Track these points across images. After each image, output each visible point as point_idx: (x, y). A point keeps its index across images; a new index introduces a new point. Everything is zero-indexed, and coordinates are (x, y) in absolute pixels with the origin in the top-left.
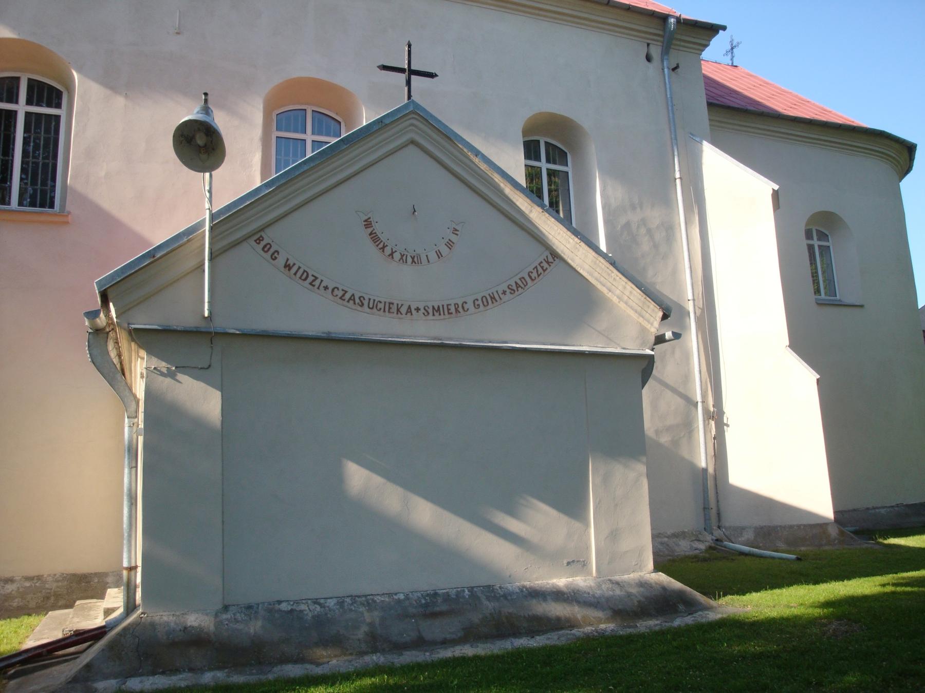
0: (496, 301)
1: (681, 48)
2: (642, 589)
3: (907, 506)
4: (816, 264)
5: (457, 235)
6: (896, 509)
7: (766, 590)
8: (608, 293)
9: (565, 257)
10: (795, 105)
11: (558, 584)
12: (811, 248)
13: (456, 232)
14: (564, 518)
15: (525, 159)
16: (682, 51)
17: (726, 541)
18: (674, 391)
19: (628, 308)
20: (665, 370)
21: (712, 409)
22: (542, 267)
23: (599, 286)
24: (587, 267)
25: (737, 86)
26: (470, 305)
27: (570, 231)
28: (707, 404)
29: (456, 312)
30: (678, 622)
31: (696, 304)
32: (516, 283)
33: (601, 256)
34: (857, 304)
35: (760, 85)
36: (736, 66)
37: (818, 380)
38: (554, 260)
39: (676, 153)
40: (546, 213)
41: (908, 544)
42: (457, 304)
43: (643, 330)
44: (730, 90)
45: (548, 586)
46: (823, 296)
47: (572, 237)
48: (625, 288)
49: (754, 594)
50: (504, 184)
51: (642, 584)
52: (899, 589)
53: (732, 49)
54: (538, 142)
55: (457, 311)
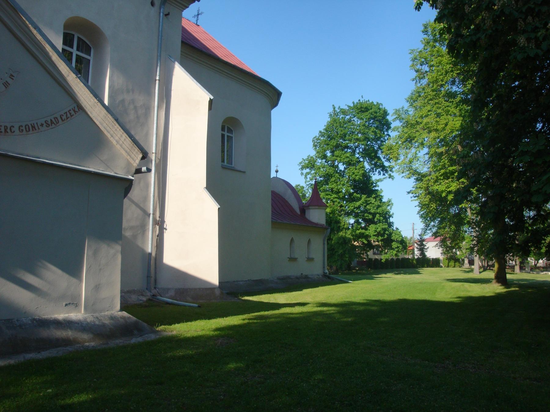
0: (36, 130)
1: (173, 4)
2: (112, 321)
3: (254, 281)
4: (224, 146)
5: (13, 79)
6: (248, 282)
7: (183, 322)
8: (110, 138)
9: (87, 110)
10: (227, 55)
11: (58, 318)
12: (223, 136)
13: (11, 77)
14: (66, 276)
15: (63, 44)
16: (173, 6)
17: (158, 296)
18: (137, 205)
19: (122, 149)
20: (135, 193)
21: (158, 219)
22: (70, 114)
23: (106, 132)
24: (99, 119)
25: (198, 37)
26: (16, 129)
27: (92, 94)
28: (155, 215)
29: (5, 132)
30: (134, 341)
31: (157, 156)
32: (51, 120)
33: (110, 113)
34: (242, 170)
35: (210, 40)
36: (199, 25)
37: (219, 208)
38: (79, 111)
39: (159, 65)
40: (78, 79)
41: (253, 300)
42: (7, 127)
43: (129, 164)
44: (194, 37)
45: (51, 319)
46: (226, 163)
47: (93, 98)
48: (122, 136)
49: (177, 325)
50: (52, 53)
51: (112, 318)
52: (251, 321)
53: (198, 15)
54: (73, 35)
55: (6, 131)
